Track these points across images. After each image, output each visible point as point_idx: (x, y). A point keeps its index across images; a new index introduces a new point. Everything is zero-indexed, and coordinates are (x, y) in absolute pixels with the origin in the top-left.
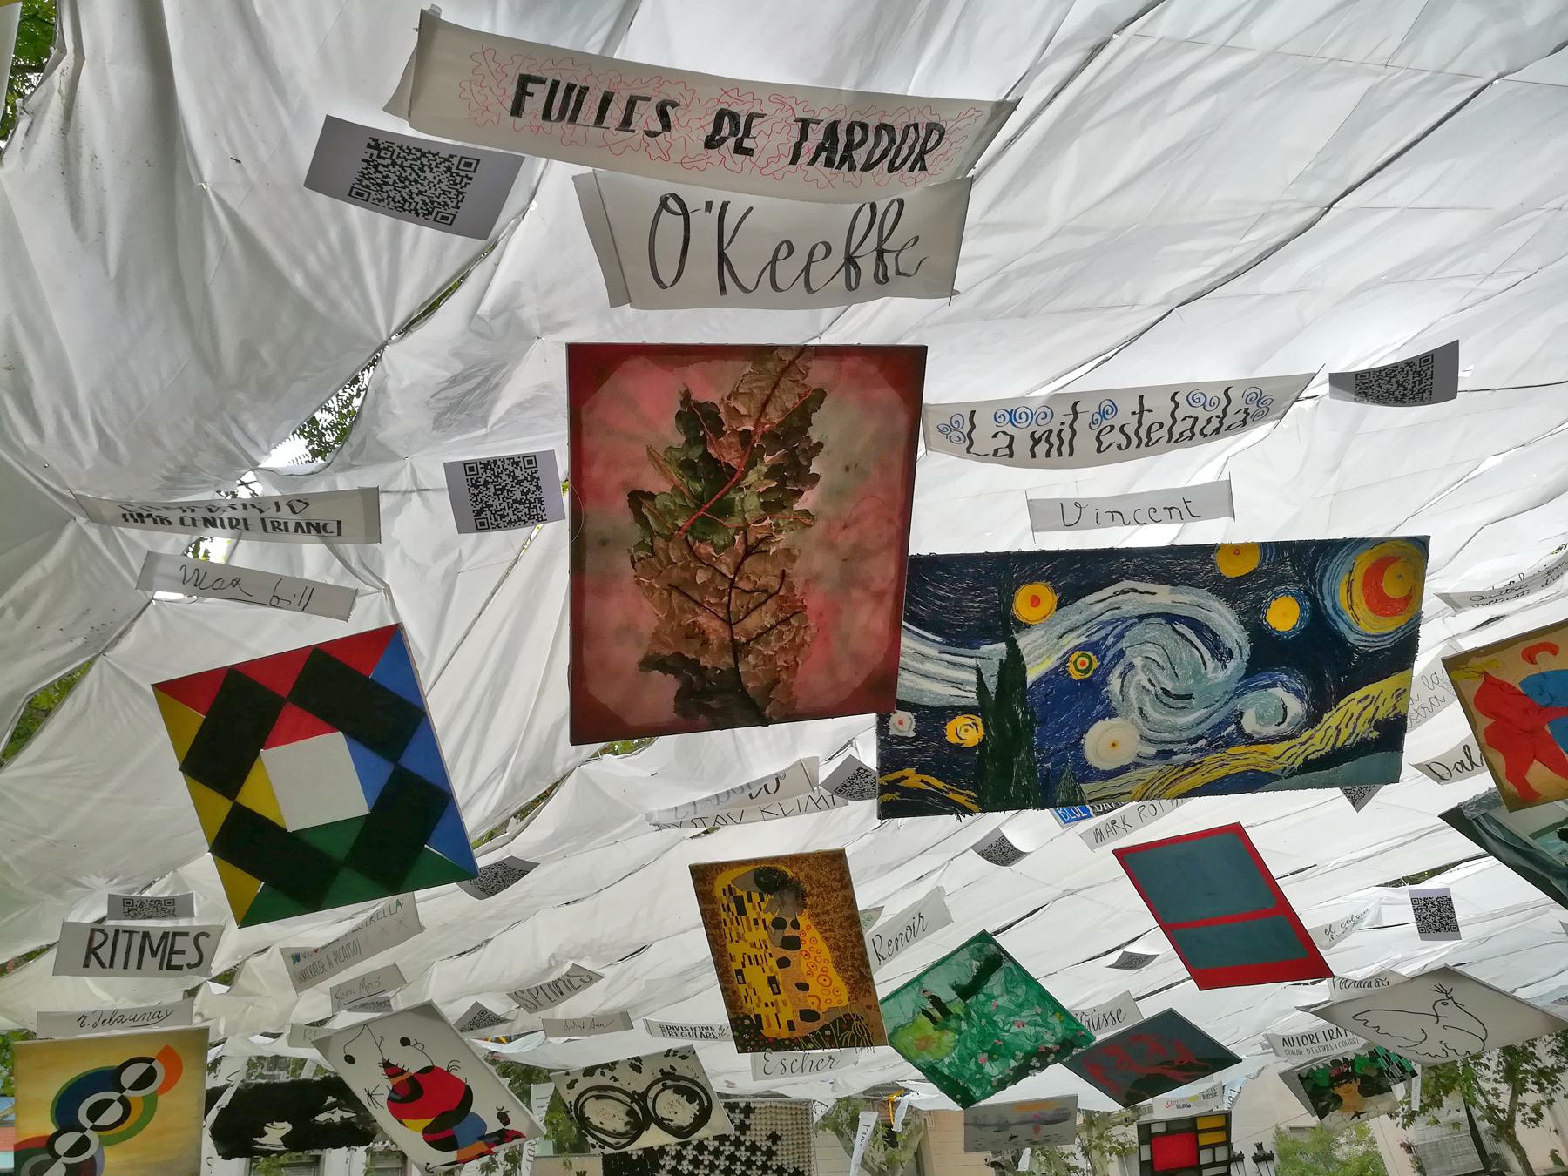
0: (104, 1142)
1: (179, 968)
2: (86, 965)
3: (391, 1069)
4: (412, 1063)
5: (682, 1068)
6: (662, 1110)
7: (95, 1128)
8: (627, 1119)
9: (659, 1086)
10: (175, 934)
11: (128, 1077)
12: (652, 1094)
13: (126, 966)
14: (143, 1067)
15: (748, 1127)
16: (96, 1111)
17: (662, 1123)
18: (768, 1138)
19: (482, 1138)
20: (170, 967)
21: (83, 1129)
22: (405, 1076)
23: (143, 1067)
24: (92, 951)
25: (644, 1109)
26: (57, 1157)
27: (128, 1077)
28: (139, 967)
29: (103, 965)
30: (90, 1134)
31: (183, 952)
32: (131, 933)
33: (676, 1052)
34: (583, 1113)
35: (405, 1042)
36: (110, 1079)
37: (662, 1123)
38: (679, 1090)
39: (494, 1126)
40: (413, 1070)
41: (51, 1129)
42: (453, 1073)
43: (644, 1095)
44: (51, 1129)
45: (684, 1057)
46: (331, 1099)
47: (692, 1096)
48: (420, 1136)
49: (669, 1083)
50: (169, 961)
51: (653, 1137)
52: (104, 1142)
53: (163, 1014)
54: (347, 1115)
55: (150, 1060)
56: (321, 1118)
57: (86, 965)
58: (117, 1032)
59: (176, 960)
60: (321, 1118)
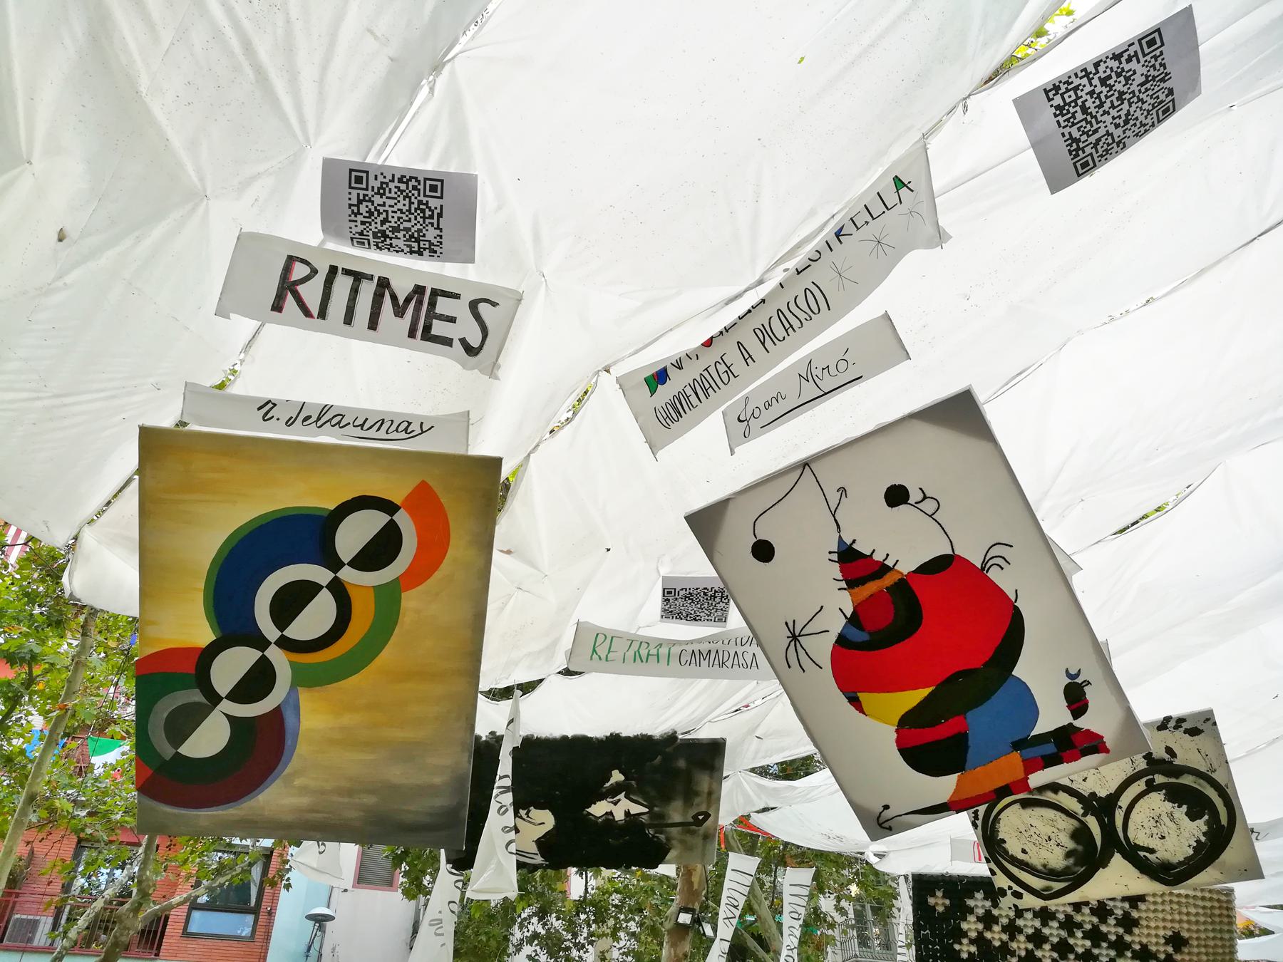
0: (303, 678)
1: (447, 342)
2: (277, 307)
3: (855, 565)
4: (905, 546)
5: (1188, 752)
6: (1139, 832)
7: (285, 643)
8: (1071, 845)
9: (1139, 786)
10: (435, 293)
11: (353, 535)
12: (1124, 801)
13: (348, 319)
14: (378, 520)
15: (1136, 923)
16: (292, 601)
17: (1137, 858)
18: (1168, 941)
19: (1018, 745)
20: (428, 336)
21: (261, 643)
22: (888, 580)
23: (378, 520)
24: (287, 287)
25: (1108, 829)
26: (214, 699)
27: (353, 535)
28: (373, 325)
29: (307, 313)
30: (276, 656)
31: (452, 320)
32: (358, 277)
33: (1181, 721)
34: (994, 831)
35: (897, 496)
36: (308, 534)
37: (1137, 858)
38: (1175, 794)
39: (1052, 716)
40: (907, 564)
41: (204, 635)
42: (994, 574)
43: (1113, 799)
44: (204, 635)
45: (1194, 732)
46: (617, 777)
47: (1195, 804)
48: (889, 734)
49: (1160, 779)
50: (427, 328)
51: (1115, 880)
52: (303, 678)
53: (415, 427)
54: (636, 809)
55: (388, 507)
56: (599, 809)
57: (277, 307)
58: (327, 437)
59: (438, 328)
60: (599, 809)
